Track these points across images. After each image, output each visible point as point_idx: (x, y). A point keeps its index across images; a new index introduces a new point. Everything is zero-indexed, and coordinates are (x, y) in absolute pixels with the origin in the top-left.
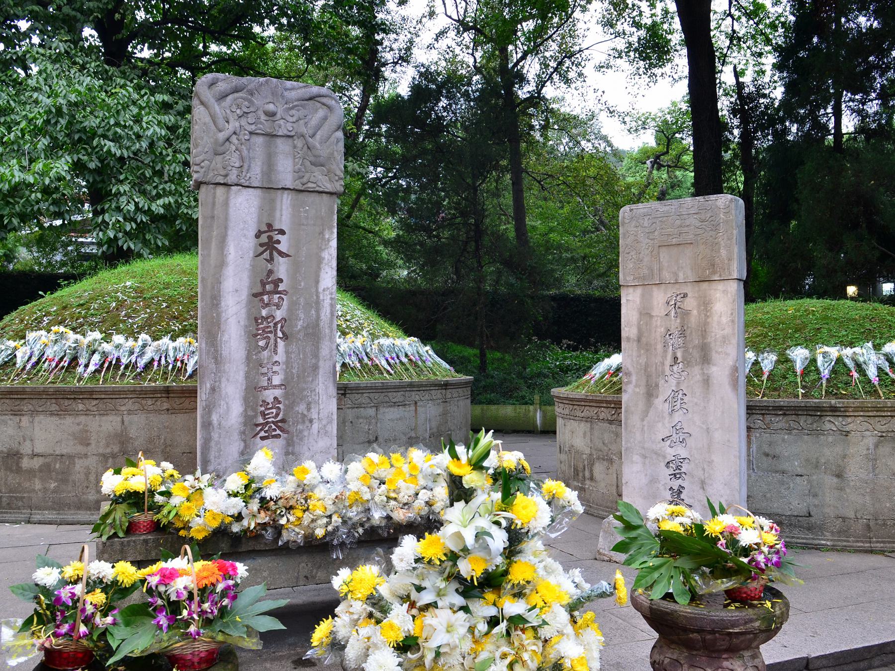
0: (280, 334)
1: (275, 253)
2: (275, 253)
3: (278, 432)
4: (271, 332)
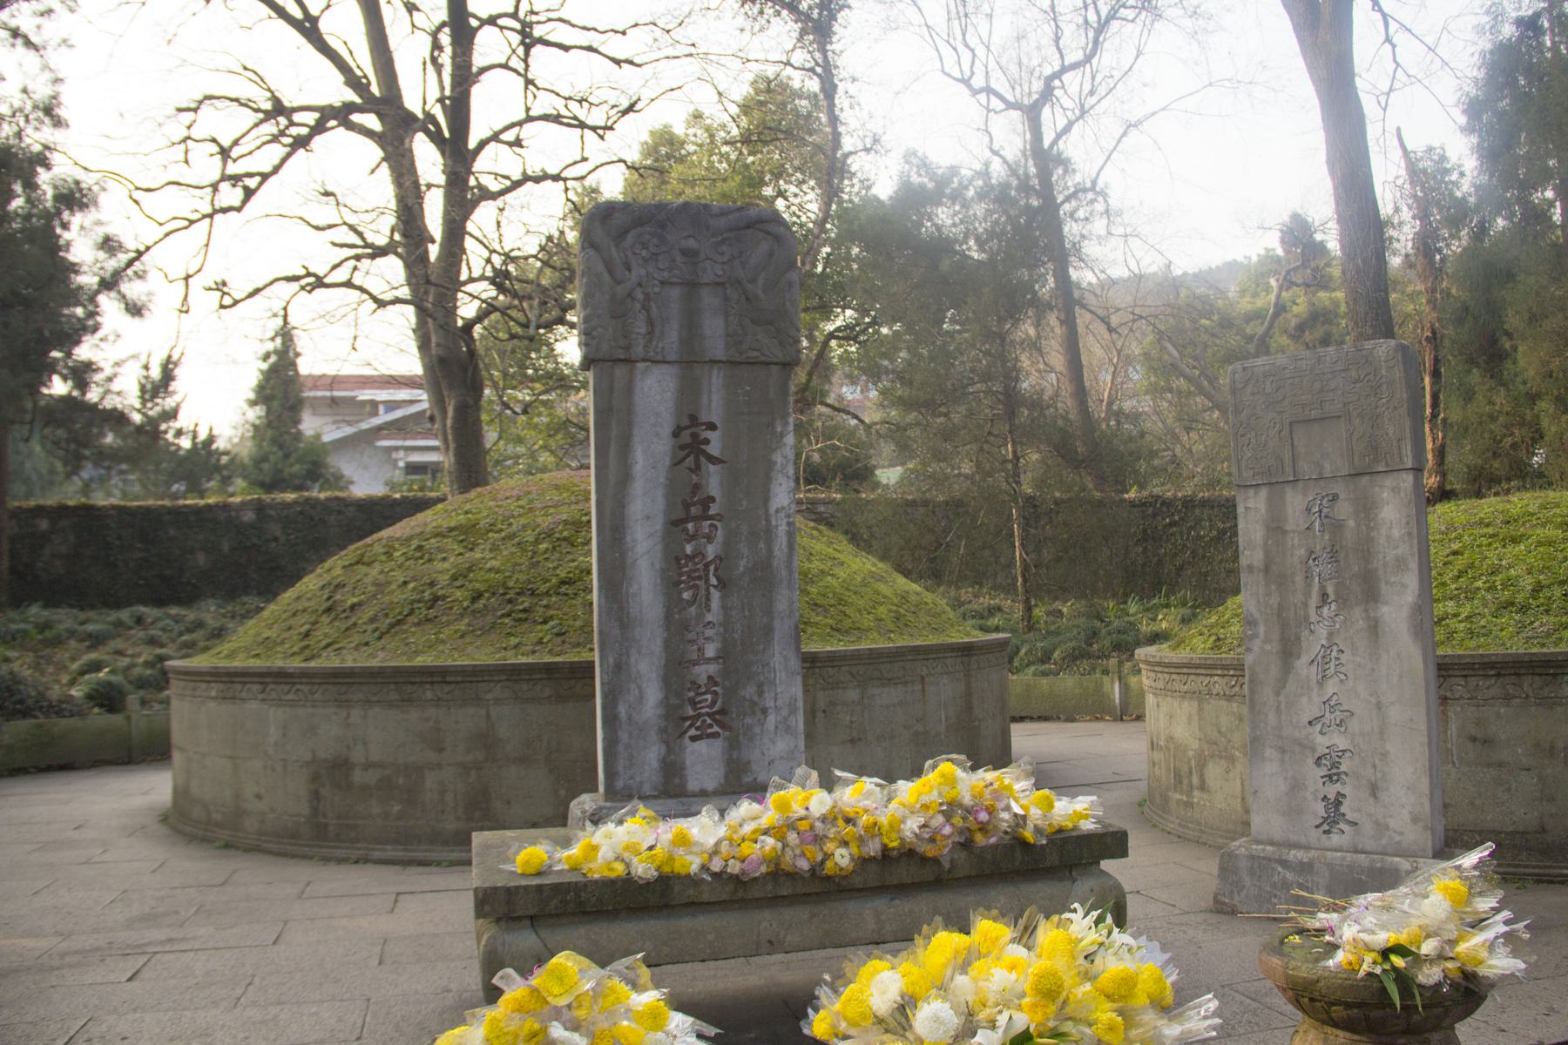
0: (714, 581)
1: (703, 460)
2: (703, 460)
3: (716, 729)
4: (699, 578)
